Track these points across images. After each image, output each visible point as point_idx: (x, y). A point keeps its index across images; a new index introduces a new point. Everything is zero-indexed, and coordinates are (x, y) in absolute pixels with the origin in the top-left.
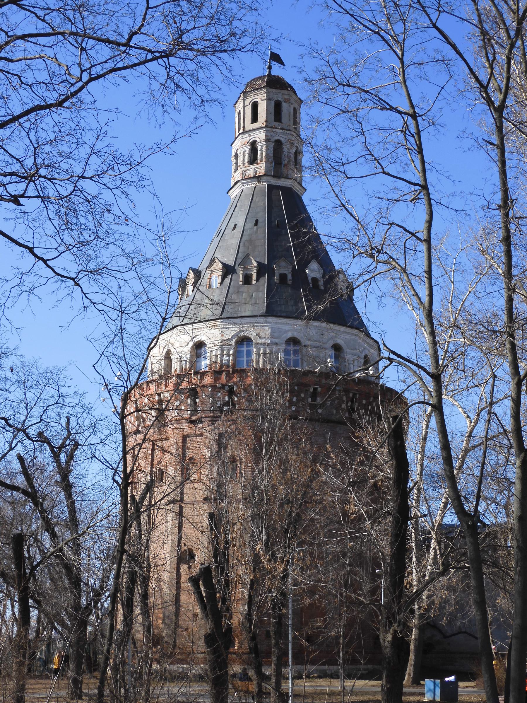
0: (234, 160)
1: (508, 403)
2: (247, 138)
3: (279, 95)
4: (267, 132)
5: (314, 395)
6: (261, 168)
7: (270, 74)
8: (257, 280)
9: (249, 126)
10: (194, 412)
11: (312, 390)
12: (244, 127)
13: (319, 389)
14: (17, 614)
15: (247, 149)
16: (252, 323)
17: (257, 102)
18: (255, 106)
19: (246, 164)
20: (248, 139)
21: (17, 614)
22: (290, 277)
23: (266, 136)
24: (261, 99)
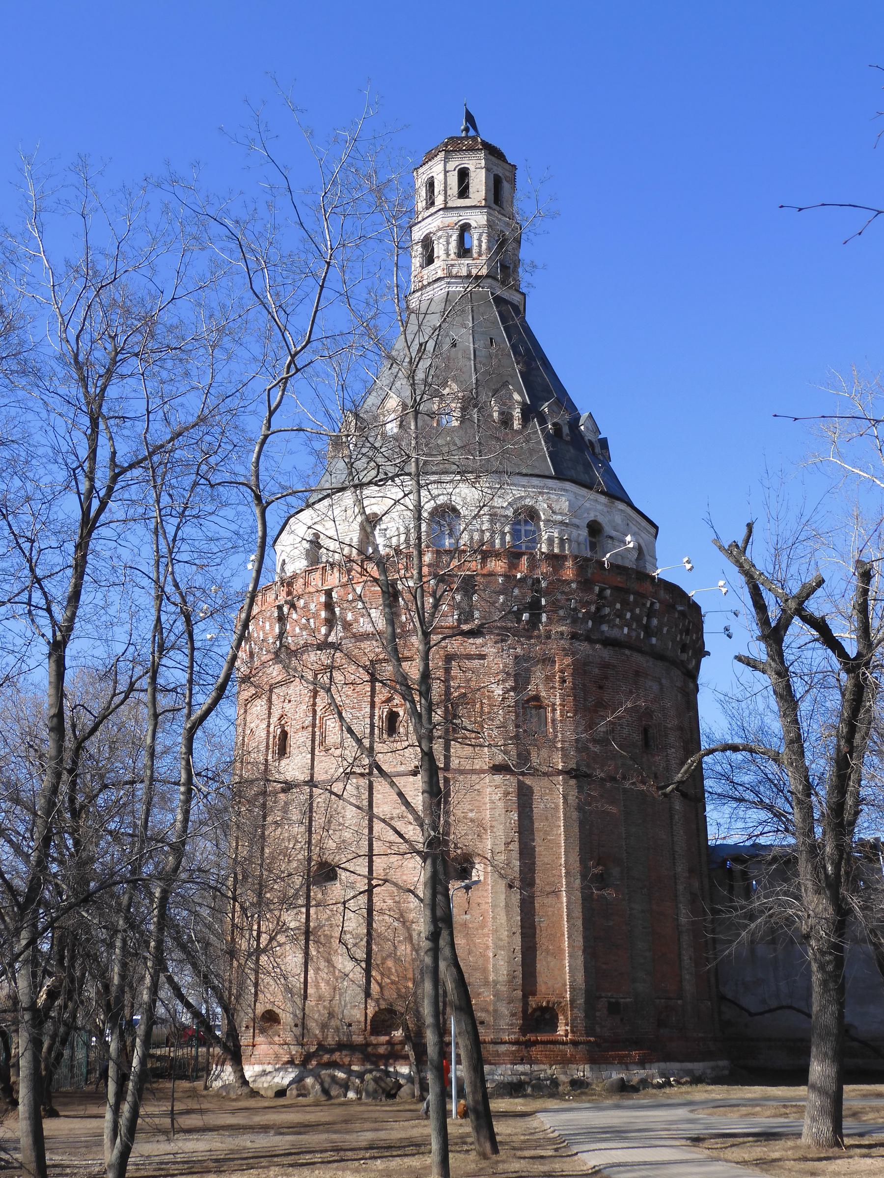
2: (453, 218)
4: (489, 214)
5: (651, 613)
6: (479, 265)
10: (467, 616)
11: (648, 605)
13: (657, 606)
14: (101, 988)
16: (541, 487)
17: (468, 169)
18: (463, 174)
19: (453, 256)
20: (456, 219)
21: (101, 988)
23: (488, 220)
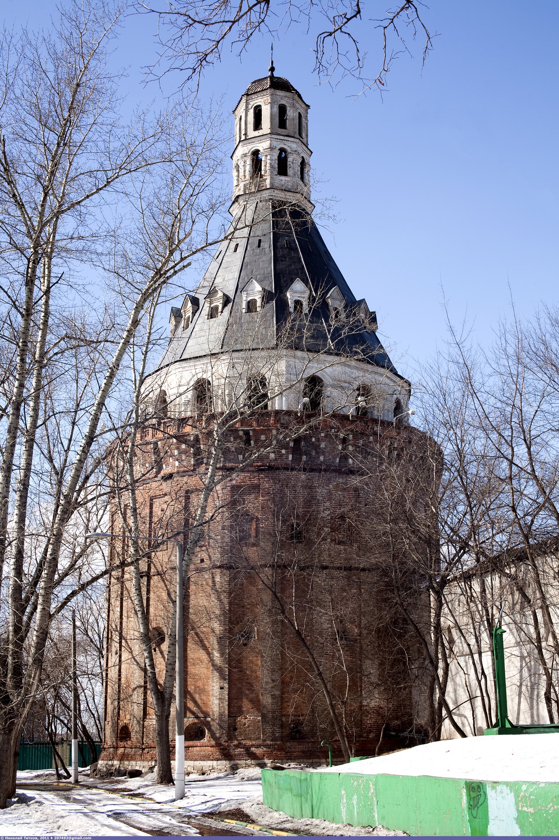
0: (235, 173)
1: (112, 596)
3: (282, 97)
7: (272, 77)
8: (263, 306)
9: (252, 133)
12: (246, 134)
15: (249, 161)
17: (260, 106)
22: (305, 303)
24: (265, 102)
